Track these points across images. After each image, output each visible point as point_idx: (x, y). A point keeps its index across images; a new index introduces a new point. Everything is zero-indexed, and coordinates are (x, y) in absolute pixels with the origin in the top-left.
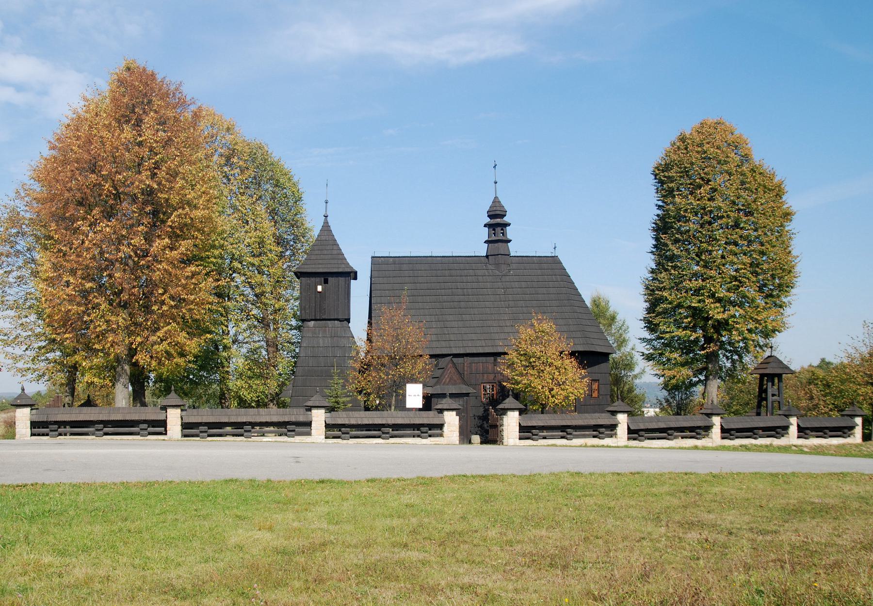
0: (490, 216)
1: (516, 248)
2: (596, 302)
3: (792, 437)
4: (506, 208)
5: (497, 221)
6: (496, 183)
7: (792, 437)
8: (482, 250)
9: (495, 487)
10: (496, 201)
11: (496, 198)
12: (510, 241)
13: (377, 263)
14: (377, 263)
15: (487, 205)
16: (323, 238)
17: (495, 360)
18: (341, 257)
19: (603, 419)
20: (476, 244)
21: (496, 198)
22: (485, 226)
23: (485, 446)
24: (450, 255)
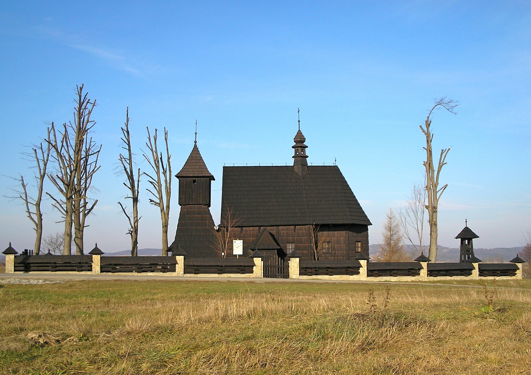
1: (311, 162)
3: (362, 276)
5: (300, 143)
7: (362, 276)
8: (291, 162)
10: (299, 133)
12: (308, 157)
13: (227, 171)
14: (227, 171)
16: (194, 155)
17: (295, 228)
20: (285, 158)
22: (293, 147)
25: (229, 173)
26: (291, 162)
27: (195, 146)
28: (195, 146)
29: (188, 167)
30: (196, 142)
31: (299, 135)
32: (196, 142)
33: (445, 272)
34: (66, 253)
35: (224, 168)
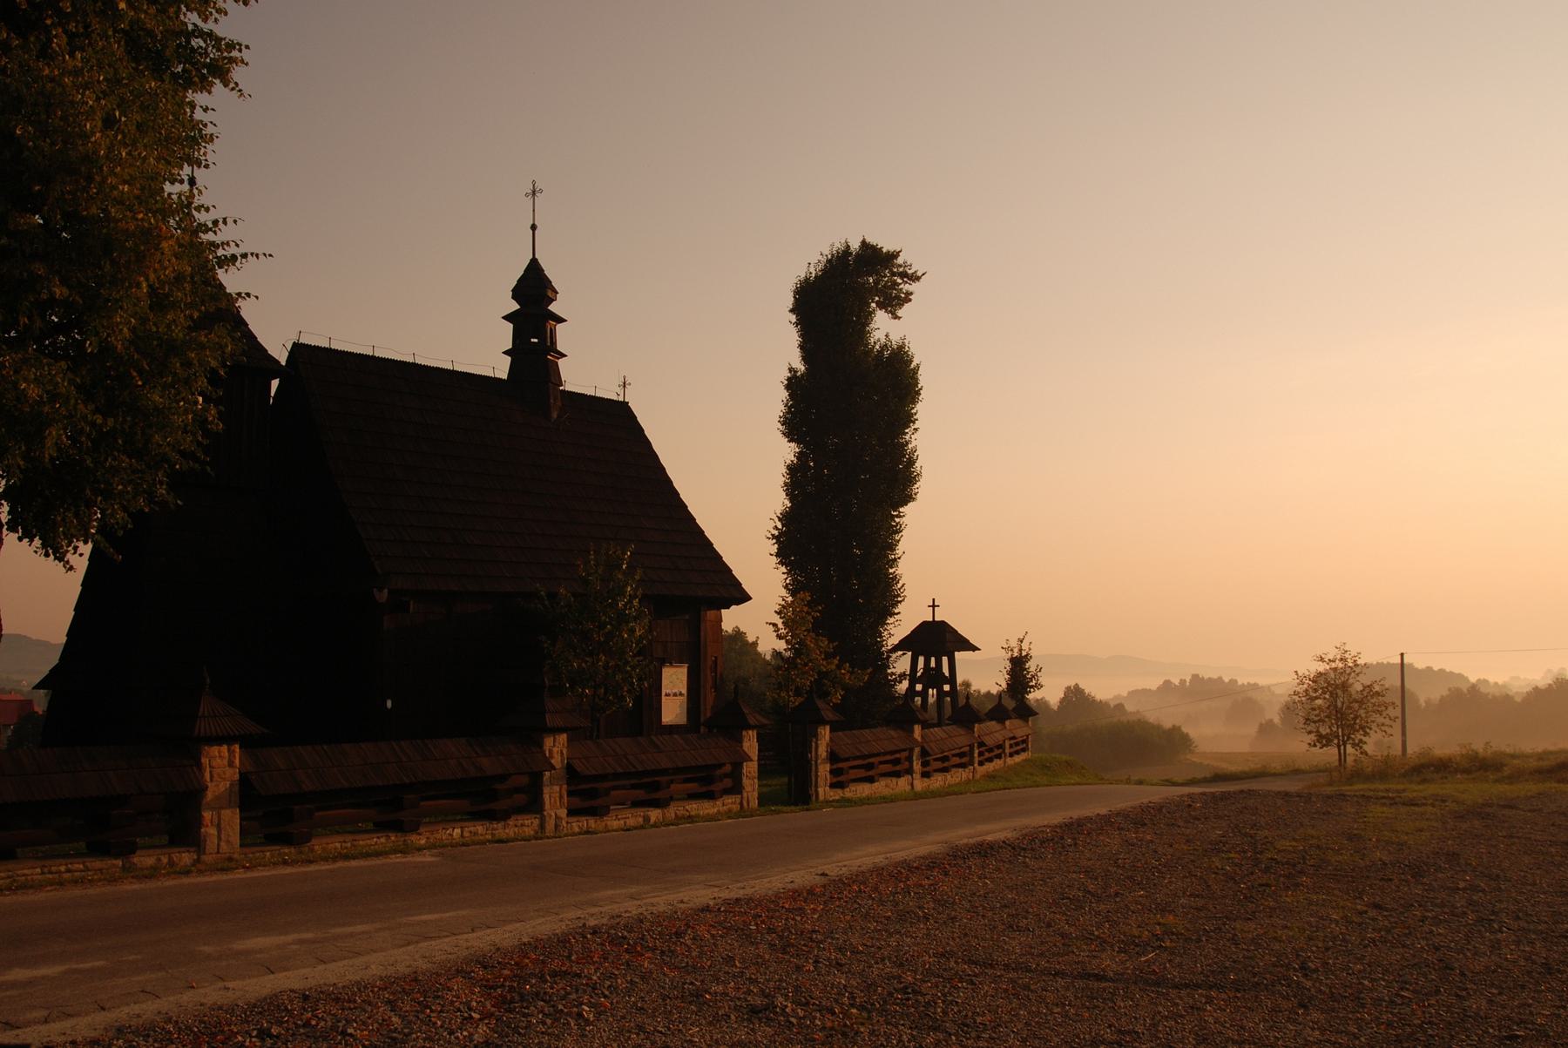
6: (934, 606)
8: (499, 367)
10: (534, 269)
20: (486, 353)
26: (499, 367)
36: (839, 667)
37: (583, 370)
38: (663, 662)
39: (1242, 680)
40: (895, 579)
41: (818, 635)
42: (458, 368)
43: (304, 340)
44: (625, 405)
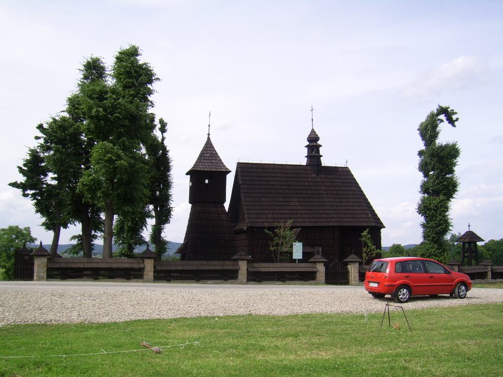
0: (308, 141)
1: (326, 162)
2: (47, 175)
4: (319, 136)
6: (469, 226)
8: (303, 161)
9: (499, 287)
10: (313, 131)
11: (313, 129)
12: (322, 156)
15: (8, 186)
18: (211, 149)
19: (227, 265)
20: (299, 157)
21: (313, 129)
23: (384, 224)
24: (273, 163)
25: (243, 168)
26: (303, 161)
27: (209, 138)
28: (209, 138)
29: (198, 164)
30: (209, 135)
31: (313, 133)
32: (209, 135)
33: (178, 274)
34: (468, 230)
35: (239, 163)
36: (122, 153)
37: (327, 161)
38: (114, 214)
39: (171, 164)
40: (168, 176)
41: (113, 70)
42: (276, 163)
43: (240, 162)
44: (347, 168)
